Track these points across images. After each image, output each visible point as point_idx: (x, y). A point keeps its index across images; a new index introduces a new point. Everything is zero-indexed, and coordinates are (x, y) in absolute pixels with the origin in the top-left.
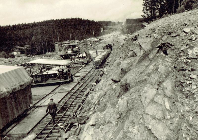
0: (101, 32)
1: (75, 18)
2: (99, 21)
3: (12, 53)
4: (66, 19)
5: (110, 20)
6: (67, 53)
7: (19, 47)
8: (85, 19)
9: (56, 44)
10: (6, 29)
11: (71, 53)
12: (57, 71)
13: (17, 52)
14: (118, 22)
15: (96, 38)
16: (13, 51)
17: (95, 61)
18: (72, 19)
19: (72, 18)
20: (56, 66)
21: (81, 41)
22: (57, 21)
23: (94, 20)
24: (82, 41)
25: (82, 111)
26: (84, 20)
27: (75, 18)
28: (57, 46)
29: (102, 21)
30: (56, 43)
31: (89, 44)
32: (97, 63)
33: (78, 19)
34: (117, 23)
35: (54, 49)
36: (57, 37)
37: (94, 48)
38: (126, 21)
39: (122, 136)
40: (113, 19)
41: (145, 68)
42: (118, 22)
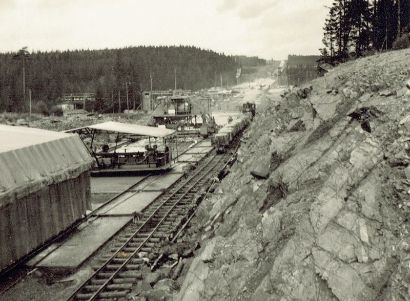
1: (187, 46)
2: (234, 55)
6: (165, 113)
9: (146, 94)
14: (272, 60)
24: (198, 92)
27: (187, 46)
30: (146, 92)
33: (193, 47)
42: (272, 60)
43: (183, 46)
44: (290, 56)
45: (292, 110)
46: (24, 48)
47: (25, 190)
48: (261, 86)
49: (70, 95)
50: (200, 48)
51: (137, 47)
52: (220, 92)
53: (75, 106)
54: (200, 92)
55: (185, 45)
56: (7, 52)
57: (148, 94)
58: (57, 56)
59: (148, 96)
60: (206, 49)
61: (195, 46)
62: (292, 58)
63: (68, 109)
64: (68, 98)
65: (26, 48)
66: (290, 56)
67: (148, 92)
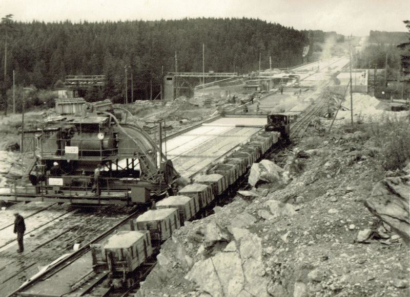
0: (302, 55)
1: (251, 19)
2: (307, 30)
3: (55, 92)
4: (224, 19)
5: (320, 29)
6: (59, 153)
7: (78, 78)
8: (273, 22)
9: (169, 79)
10: (94, 28)
11: (77, 158)
12: (301, 78)
13: (66, 91)
14: (352, 36)
15: (283, 71)
16: (60, 87)
17: (106, 251)
18: (244, 21)
19: (245, 17)
20: (27, 199)
21: (244, 76)
22: (220, 21)
23: (292, 27)
24: (247, 75)
25: (282, 176)
26: (270, 25)
27: (251, 19)
28: (170, 86)
29: (314, 31)
30: (167, 77)
31: (256, 87)
32: (113, 265)
33: (258, 20)
34: (349, 37)
35: (161, 92)
36: (202, 59)
37: (247, 111)
38: (369, 34)
39: (330, 278)
40: (326, 29)
41: (383, 228)
42: (352, 36)
43: (247, 19)
44: (372, 32)
45: (272, 250)
46: (7, 16)
47: (20, 193)
48: (329, 69)
49: (74, 78)
50: (43, 22)
51: (195, 18)
52: (276, 76)
53: (76, 92)
54: (249, 75)
55: (249, 18)
56: (126, 20)
57: (171, 79)
58: (94, 28)
59: (170, 82)
60: (273, 22)
61: (205, 17)
62: (374, 35)
63: (66, 97)
64: (72, 81)
65: (10, 16)
66: (372, 32)
67: (171, 77)
